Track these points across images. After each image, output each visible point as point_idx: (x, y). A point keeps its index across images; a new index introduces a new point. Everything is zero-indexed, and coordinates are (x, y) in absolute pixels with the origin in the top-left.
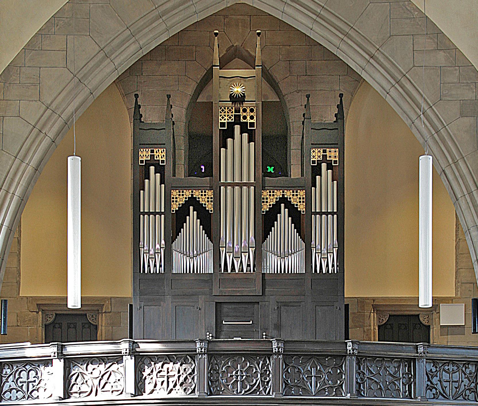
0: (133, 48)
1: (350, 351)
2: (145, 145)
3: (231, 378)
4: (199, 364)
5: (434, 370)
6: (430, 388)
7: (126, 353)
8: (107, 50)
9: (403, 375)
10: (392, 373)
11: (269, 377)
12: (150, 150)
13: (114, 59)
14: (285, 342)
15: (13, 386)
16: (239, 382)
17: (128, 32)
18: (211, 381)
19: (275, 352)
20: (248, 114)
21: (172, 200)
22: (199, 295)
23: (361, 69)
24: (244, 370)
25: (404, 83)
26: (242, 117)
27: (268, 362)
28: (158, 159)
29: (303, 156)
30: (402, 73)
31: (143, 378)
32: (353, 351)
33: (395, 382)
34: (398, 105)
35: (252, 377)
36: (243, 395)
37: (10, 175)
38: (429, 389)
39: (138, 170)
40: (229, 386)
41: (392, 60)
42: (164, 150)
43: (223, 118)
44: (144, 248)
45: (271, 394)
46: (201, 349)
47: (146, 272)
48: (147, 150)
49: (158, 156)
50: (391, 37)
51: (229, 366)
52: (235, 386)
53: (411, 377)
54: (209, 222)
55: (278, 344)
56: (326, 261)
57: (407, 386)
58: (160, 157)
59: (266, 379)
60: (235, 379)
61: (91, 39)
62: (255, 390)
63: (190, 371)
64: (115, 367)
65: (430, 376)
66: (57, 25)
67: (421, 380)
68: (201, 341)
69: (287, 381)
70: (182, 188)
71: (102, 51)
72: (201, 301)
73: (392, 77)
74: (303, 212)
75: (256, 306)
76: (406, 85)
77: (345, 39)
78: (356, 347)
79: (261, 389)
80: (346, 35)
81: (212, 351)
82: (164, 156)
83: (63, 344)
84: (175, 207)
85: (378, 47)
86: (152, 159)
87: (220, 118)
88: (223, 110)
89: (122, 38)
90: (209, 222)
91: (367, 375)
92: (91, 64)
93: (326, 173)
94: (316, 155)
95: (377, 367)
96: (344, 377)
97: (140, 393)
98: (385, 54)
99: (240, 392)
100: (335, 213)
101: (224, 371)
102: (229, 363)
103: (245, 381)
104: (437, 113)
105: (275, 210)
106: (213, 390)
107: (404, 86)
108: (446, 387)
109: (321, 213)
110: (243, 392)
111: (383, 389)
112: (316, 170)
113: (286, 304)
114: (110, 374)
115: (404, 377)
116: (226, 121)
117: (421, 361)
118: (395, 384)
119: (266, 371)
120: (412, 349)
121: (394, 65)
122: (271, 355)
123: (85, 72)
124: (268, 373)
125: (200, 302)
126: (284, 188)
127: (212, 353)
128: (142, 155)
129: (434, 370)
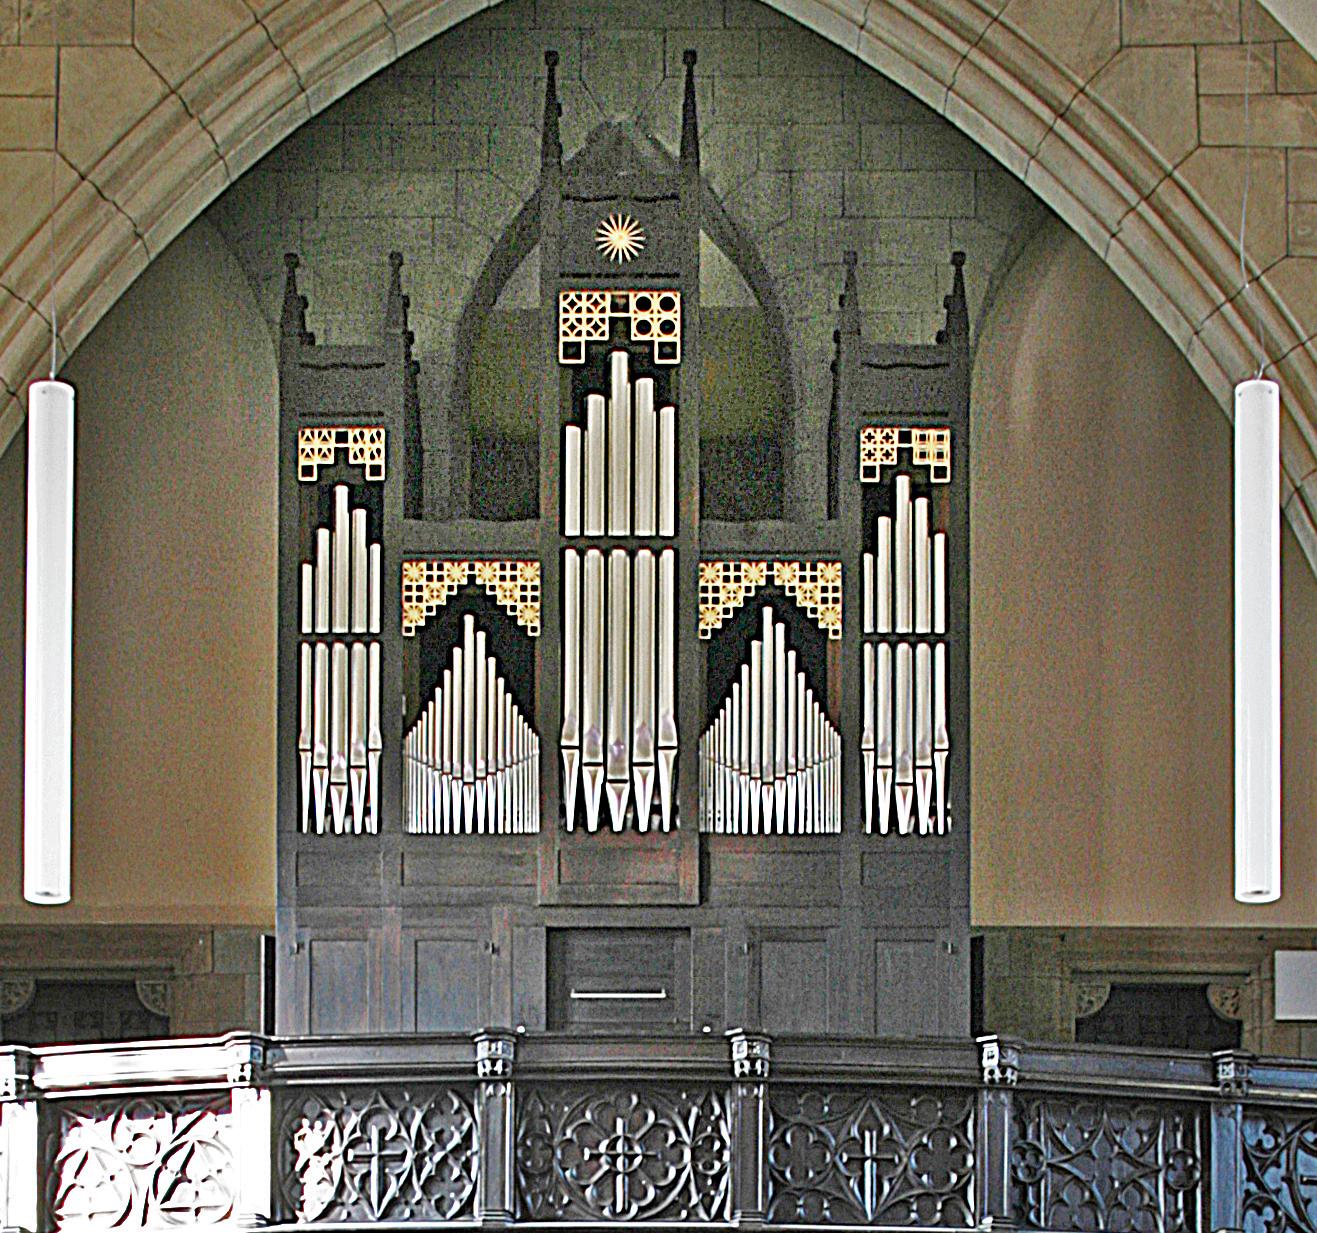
1: (992, 1072)
2: (319, 419)
3: (594, 1164)
4: (486, 1115)
5: (1269, 1142)
7: (242, 1079)
8: (190, 89)
9: (1166, 1157)
10: (1130, 1151)
11: (720, 1158)
12: (334, 432)
13: (213, 121)
14: (774, 1042)
16: (619, 1178)
17: (259, 34)
18: (528, 1176)
19: (743, 1074)
20: (656, 316)
21: (406, 594)
22: (492, 902)
23: (1027, 157)
24: (638, 1136)
25: (1168, 201)
26: (634, 325)
27: (717, 1110)
28: (360, 461)
29: (836, 446)
30: (1161, 168)
31: (298, 1167)
32: (1003, 1072)
33: (1142, 1181)
34: (1146, 271)
35: (664, 1159)
36: (633, 1220)
38: (1252, 1206)
40: (588, 1192)
41: (1129, 125)
42: (379, 434)
43: (572, 327)
44: (312, 750)
45: (727, 1214)
46: (493, 1064)
47: (320, 830)
48: (325, 432)
49: (362, 451)
50: (1125, 52)
51: (587, 1124)
52: (608, 1192)
53: (1194, 1166)
54: (525, 668)
55: (750, 1047)
56: (908, 796)
57: (1180, 1196)
58: (367, 454)
59: (712, 1167)
60: (606, 1167)
61: (137, 57)
62: (674, 1202)
63: (457, 1139)
64: (209, 1124)
65: (1256, 1161)
66: (29, 15)
67: (1227, 1175)
68: (493, 1036)
69: (782, 1174)
70: (436, 556)
71: (173, 97)
72: (498, 923)
73: (1129, 181)
74: (836, 632)
75: (679, 941)
76: (1173, 206)
77: (975, 55)
78: (1012, 1058)
79: (695, 1199)
80: (978, 42)
81: (530, 1071)
82: (378, 451)
83: (36, 1051)
84: (414, 617)
85: (1081, 82)
86: (342, 465)
87: (563, 327)
88: (572, 304)
89: (238, 51)
91: (1048, 1153)
93: (911, 509)
94: (878, 448)
95: (1082, 1132)
96: (970, 1162)
97: (288, 1216)
98: (1106, 105)
99: (625, 1211)
100: (940, 638)
101: (570, 1141)
102: (588, 1115)
103: (641, 1174)
104: (1279, 300)
105: (743, 627)
106: (534, 1200)
107: (1169, 210)
108: (1307, 1202)
109: (894, 639)
110: (634, 1209)
111: (1103, 1205)
112: (880, 501)
113: (777, 935)
114: (192, 1151)
115: (1169, 1167)
116: (583, 339)
117: (1226, 1111)
118: (1141, 1189)
119: (710, 1140)
120: (1196, 1069)
121: (1135, 141)
122: (729, 1085)
123: (118, 163)
124: (717, 1145)
125: (497, 924)
126: (769, 556)
127: (530, 1077)
128: (308, 450)
129: (1269, 1142)
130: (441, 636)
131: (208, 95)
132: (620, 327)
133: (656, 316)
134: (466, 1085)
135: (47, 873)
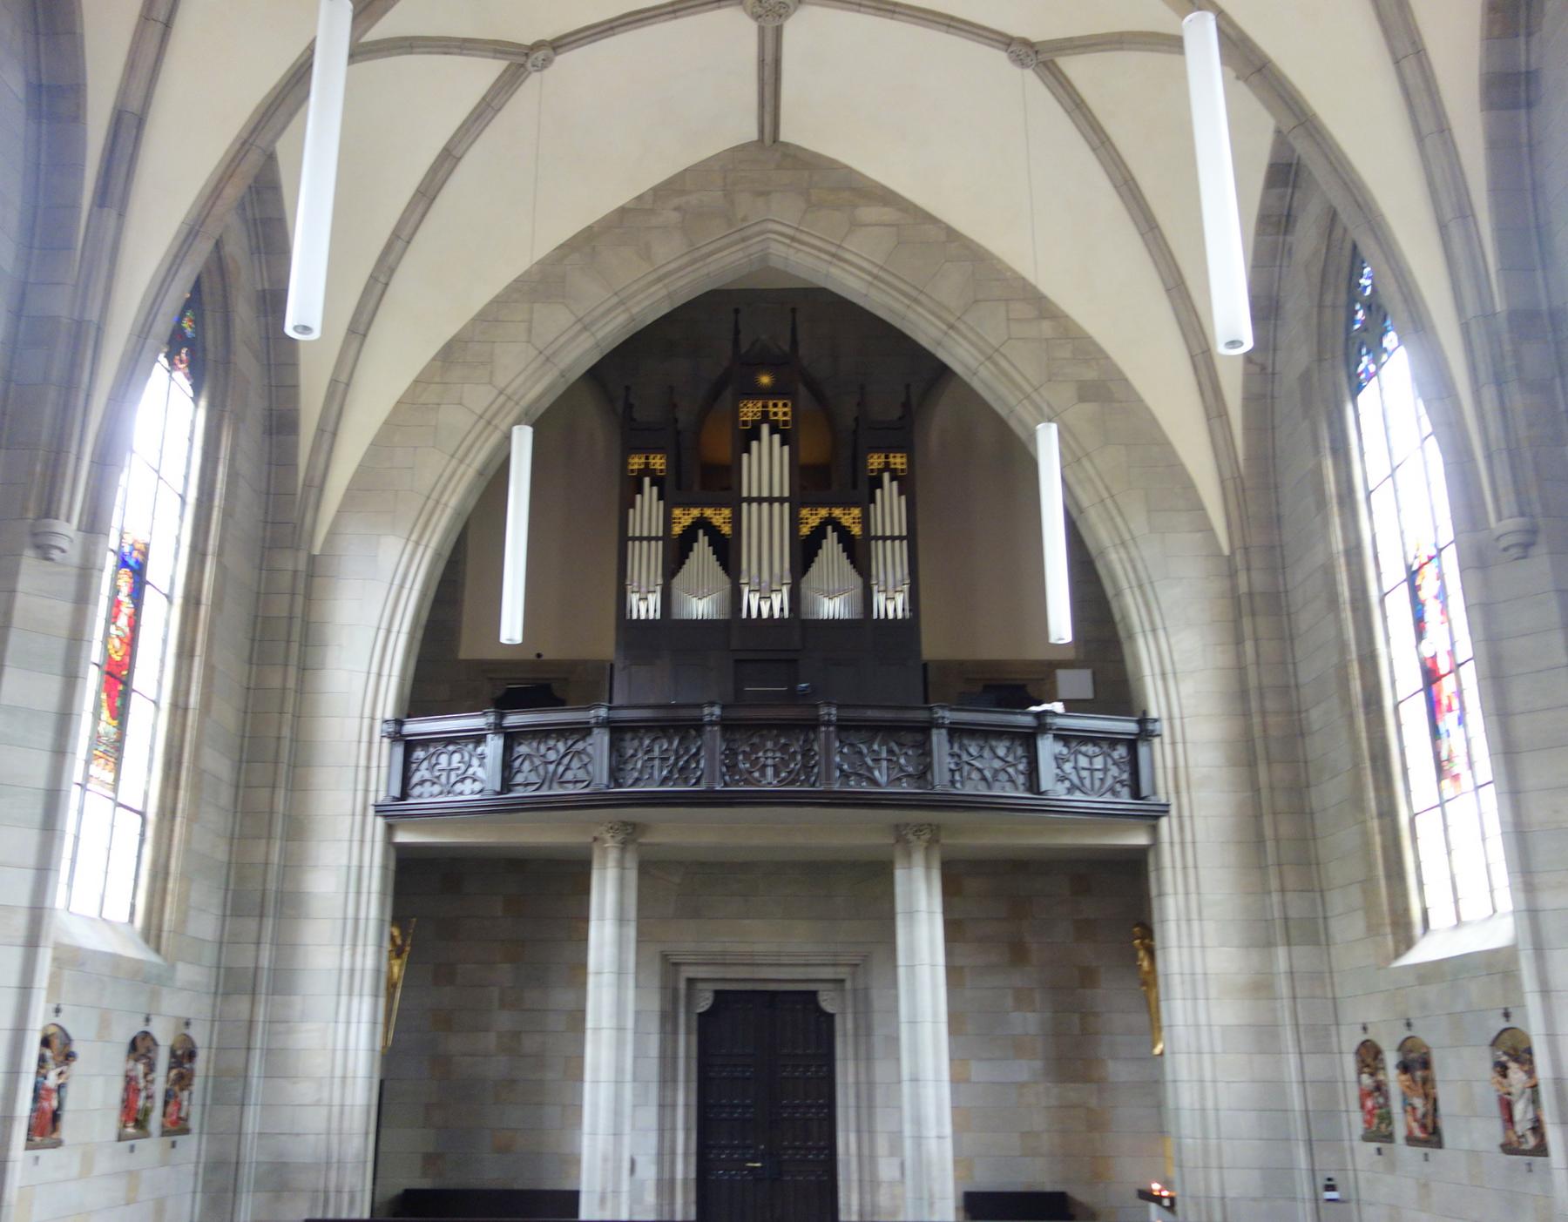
0: (622, 318)
6: (1062, 779)
15: (427, 775)
17: (615, 300)
37: (443, 480)
39: (695, 1018)
56: (891, 604)
65: (1059, 760)
70: (687, 505)
90: (727, 552)
92: (563, 339)
109: (884, 538)
130: (689, 537)
131: (593, 323)
132: (765, 414)
133: (780, 409)
134: (699, 726)
135: (511, 629)
